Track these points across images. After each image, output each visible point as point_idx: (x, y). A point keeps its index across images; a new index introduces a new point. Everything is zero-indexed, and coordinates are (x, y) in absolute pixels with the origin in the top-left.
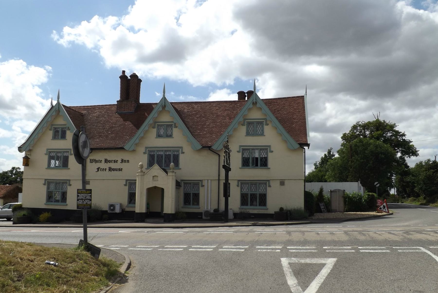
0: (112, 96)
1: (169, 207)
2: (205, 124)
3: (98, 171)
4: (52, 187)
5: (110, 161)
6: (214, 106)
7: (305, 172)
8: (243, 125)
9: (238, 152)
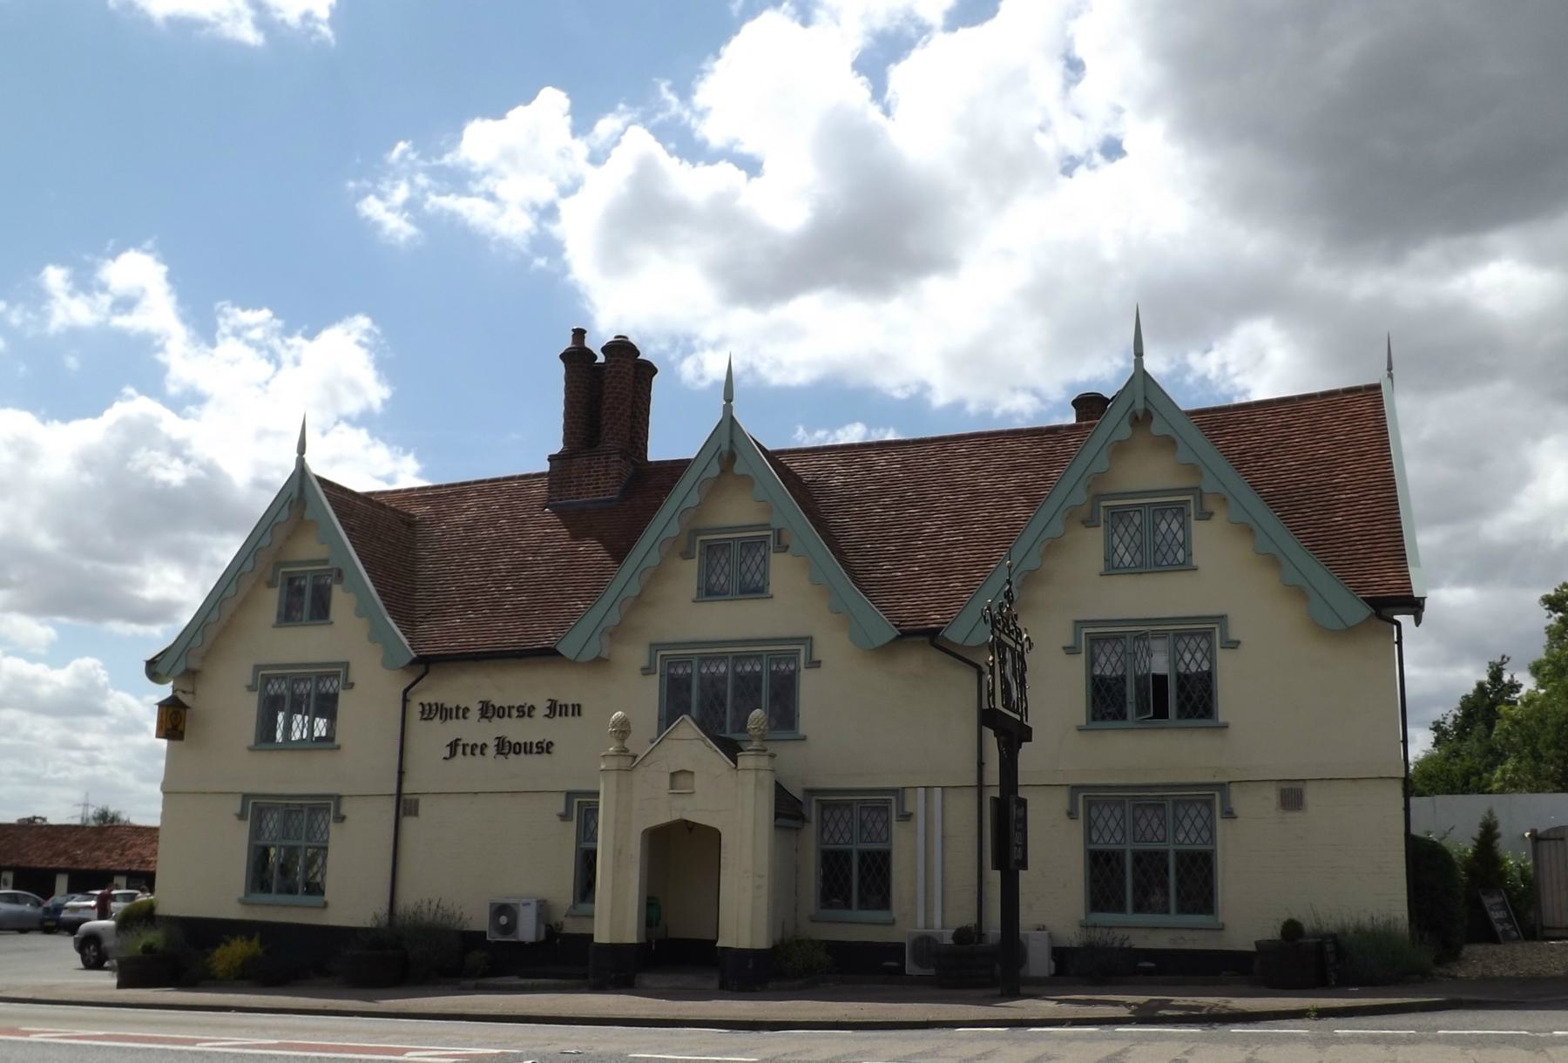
0: (526, 435)
1: (743, 915)
2: (918, 533)
3: (453, 754)
4: (272, 823)
5: (501, 712)
6: (962, 454)
7: (1405, 741)
8: (1089, 522)
9: (1071, 650)
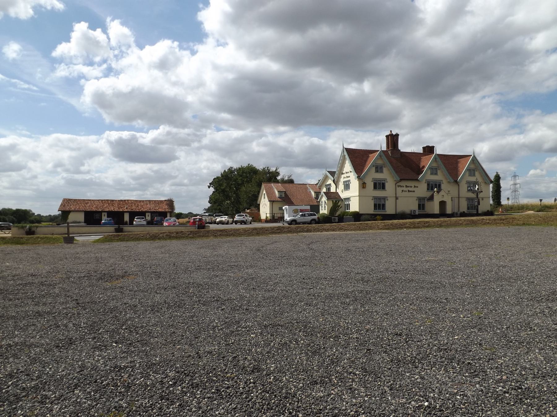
5: (408, 187)
